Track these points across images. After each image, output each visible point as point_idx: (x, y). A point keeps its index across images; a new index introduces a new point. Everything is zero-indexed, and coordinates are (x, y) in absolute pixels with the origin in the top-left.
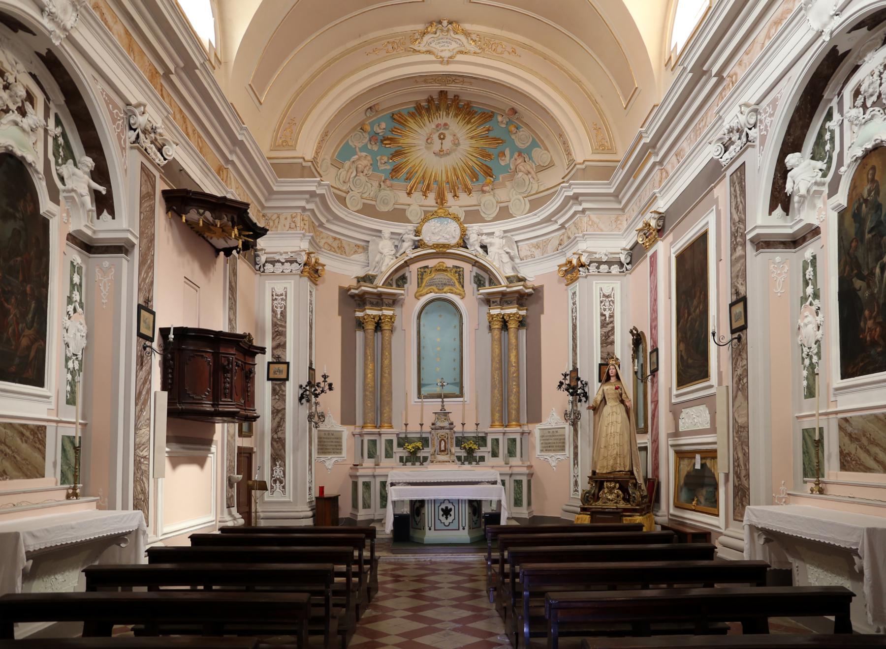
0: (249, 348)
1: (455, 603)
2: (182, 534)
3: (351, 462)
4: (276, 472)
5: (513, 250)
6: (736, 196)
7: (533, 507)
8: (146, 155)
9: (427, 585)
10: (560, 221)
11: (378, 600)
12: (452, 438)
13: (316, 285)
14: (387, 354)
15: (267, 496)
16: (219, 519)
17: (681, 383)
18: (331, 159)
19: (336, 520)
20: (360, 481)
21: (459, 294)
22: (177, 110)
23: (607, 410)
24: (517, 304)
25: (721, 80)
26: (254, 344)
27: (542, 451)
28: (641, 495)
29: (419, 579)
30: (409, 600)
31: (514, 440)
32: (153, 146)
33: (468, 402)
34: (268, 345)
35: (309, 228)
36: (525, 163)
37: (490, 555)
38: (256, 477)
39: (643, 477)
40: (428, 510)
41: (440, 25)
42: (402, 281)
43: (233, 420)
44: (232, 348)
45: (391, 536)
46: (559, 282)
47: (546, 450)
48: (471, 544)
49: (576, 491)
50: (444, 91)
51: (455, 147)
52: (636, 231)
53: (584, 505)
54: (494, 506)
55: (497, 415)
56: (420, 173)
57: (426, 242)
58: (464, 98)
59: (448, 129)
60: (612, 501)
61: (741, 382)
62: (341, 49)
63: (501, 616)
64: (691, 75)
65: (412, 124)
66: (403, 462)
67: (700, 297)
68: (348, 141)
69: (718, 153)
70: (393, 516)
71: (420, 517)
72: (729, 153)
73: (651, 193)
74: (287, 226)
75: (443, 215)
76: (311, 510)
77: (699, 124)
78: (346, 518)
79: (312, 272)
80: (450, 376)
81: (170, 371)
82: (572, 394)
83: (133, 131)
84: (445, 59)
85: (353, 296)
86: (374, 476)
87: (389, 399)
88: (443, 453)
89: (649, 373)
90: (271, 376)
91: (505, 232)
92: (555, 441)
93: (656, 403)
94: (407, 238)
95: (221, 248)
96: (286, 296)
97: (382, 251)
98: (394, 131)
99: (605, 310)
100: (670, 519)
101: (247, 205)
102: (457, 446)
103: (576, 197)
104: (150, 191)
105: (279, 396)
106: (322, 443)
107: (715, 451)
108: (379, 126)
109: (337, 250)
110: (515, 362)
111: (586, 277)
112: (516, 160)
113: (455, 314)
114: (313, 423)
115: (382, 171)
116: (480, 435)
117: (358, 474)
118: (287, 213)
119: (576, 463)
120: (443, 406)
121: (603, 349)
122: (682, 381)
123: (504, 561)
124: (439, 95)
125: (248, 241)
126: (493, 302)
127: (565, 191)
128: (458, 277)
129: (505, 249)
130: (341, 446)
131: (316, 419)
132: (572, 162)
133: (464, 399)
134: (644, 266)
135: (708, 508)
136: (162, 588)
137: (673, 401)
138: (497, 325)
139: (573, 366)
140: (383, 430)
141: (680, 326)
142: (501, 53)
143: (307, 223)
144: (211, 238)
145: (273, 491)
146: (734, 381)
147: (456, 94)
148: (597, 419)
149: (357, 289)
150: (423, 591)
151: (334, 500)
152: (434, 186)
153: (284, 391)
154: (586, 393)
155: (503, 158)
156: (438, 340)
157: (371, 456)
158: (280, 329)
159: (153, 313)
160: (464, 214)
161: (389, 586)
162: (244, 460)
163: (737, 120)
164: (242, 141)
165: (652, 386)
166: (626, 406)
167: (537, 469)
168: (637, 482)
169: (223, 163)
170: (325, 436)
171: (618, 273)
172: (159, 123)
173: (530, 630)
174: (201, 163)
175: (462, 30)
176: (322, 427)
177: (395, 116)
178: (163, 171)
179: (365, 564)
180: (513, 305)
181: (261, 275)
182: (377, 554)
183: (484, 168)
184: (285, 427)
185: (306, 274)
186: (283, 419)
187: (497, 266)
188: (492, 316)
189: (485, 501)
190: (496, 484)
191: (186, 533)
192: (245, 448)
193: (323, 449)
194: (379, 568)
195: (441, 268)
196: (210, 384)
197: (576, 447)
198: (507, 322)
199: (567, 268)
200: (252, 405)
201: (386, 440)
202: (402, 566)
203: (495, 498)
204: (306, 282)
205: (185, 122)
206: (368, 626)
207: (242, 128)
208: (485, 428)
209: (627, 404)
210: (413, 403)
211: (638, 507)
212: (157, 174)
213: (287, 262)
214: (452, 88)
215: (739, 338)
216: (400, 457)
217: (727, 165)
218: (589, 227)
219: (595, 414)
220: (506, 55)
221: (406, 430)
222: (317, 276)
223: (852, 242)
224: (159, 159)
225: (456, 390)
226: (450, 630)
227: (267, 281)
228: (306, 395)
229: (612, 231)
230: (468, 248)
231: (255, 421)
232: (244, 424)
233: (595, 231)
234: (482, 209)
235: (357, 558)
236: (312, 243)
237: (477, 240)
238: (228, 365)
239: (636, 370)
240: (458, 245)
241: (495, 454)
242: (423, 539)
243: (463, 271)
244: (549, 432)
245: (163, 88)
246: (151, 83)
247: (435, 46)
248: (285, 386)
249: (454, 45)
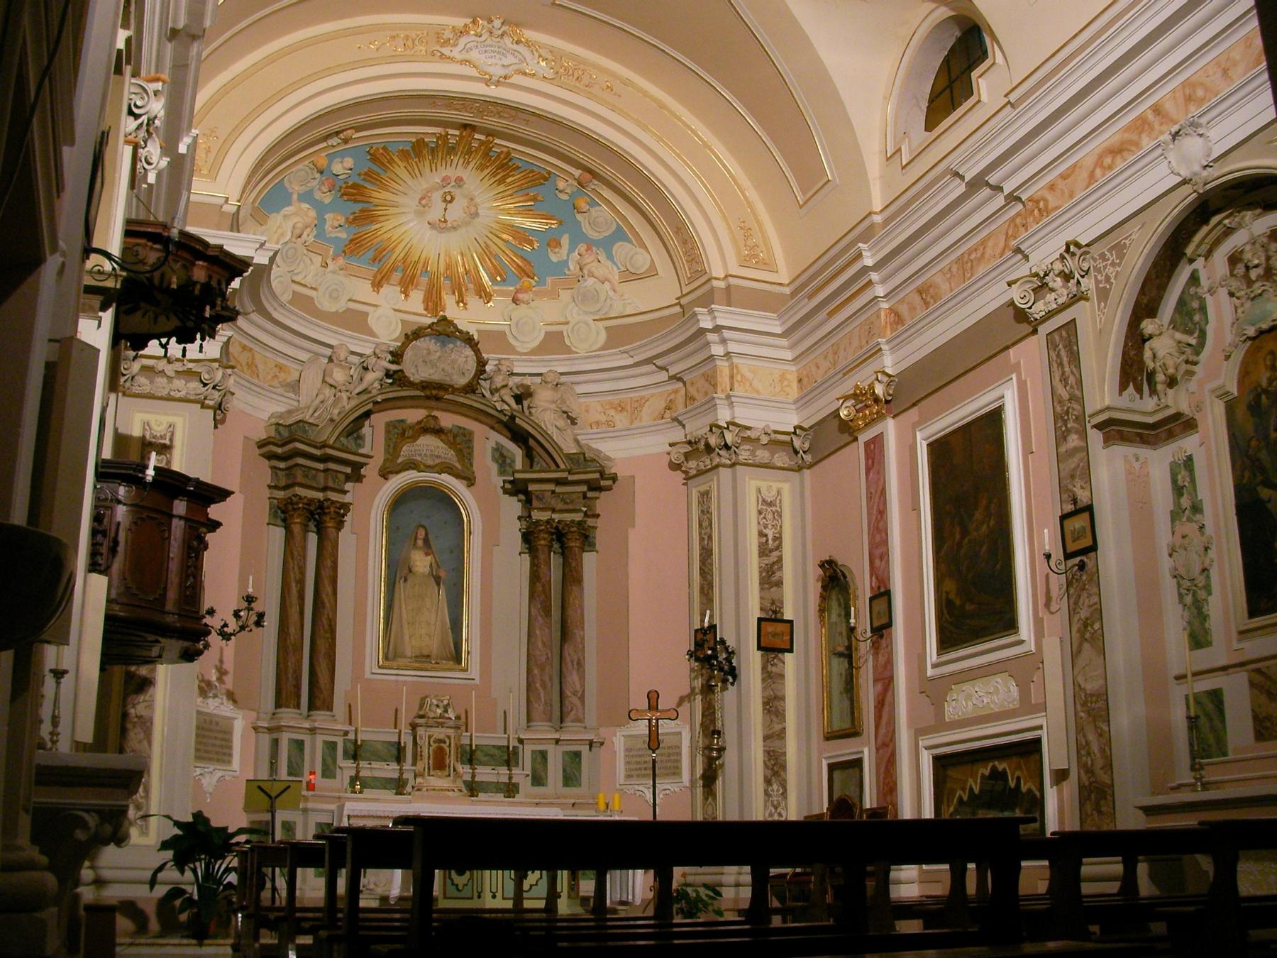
6: (1061, 365)
17: (946, 642)
27: (629, 776)
61: (1089, 628)
65: (400, 169)
83: (132, 118)
99: (766, 526)
107: (1038, 741)
130: (230, 748)
146: (1074, 629)
155: (557, 250)
201: (325, 742)
215: (1082, 566)
223: (1250, 440)
233: (746, 391)
241: (538, 780)
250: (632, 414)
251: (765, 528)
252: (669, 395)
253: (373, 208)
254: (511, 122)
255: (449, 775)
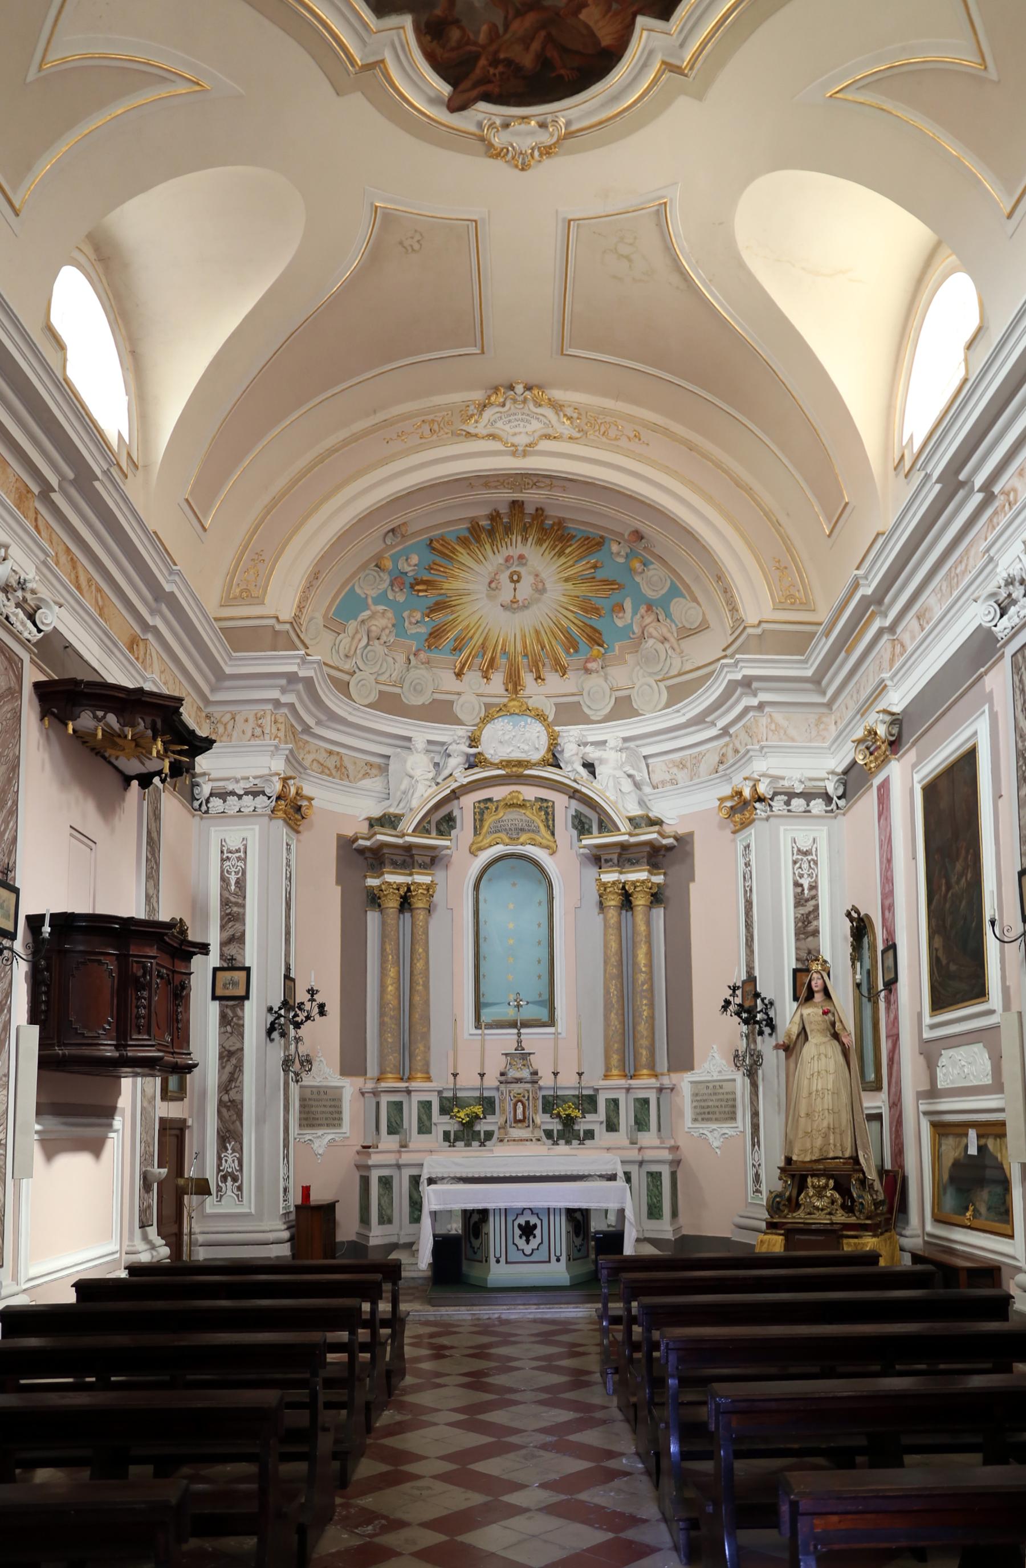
0: (181, 945)
1: (545, 1396)
2: (62, 1278)
3: (357, 1143)
4: (226, 1161)
5: (640, 771)
7: (682, 1219)
8: (7, 627)
9: (493, 1364)
10: (721, 723)
11: (405, 1391)
12: (535, 1099)
13: (298, 832)
14: (421, 950)
15: (210, 1205)
16: (125, 1248)
18: (325, 616)
19: (330, 1247)
20: (374, 1176)
21: (547, 847)
22: (61, 549)
23: (809, 1050)
24: (648, 864)
25: (989, 497)
26: (190, 938)
27: (695, 1120)
28: (873, 1200)
29: (480, 1353)
30: (461, 1391)
31: (646, 1102)
32: (19, 610)
33: (564, 1035)
34: (214, 938)
35: (286, 736)
36: (659, 624)
37: (605, 1307)
38: (191, 1172)
39: (876, 1166)
40: (494, 1228)
41: (512, 393)
42: (447, 824)
43: (152, 1072)
44: (151, 946)
45: (429, 1274)
46: (721, 827)
47: (703, 1119)
48: (572, 1287)
49: (758, 1191)
50: (518, 501)
51: (537, 595)
52: (853, 742)
53: (772, 1217)
54: (612, 1219)
55: (615, 1058)
56: (477, 640)
57: (488, 756)
58: (553, 513)
59: (525, 564)
60: (822, 1210)
62: (343, 434)
63: (628, 1421)
64: (938, 487)
65: (463, 556)
66: (449, 1141)
67: (966, 858)
68: (353, 586)
69: (990, 617)
70: (431, 1238)
71: (479, 1241)
72: (1009, 619)
73: (877, 680)
74: (249, 734)
75: (517, 711)
76: (288, 1228)
77: (956, 568)
78: (348, 1242)
79: (292, 811)
80: (532, 988)
81: (44, 989)
82: (746, 1022)
84: (520, 448)
85: (361, 851)
86: (399, 1166)
87: (425, 1030)
88: (520, 1125)
89: (881, 986)
90: (219, 992)
91: (625, 740)
92: (718, 1104)
93: (895, 1038)
94: (455, 751)
95: (132, 773)
96: (245, 852)
97: (412, 773)
98: (432, 569)
99: (801, 876)
100: (926, 1243)
101: (180, 700)
102: (544, 1111)
103: (747, 683)
104: (13, 684)
105: (233, 1027)
106: (307, 1109)
107: (1003, 1124)
108: (407, 560)
109: (334, 772)
110: (645, 965)
111: (767, 819)
112: (643, 617)
113: (540, 882)
114: (291, 1074)
115: (413, 637)
116: (585, 1092)
117: (370, 1163)
118: (249, 712)
119: (755, 1142)
120: (519, 1042)
121: (798, 943)
122: (940, 1001)
123: (633, 1320)
124: (510, 508)
125: (180, 761)
126: (606, 861)
127: (727, 672)
128: (544, 817)
129: (625, 769)
131: (297, 1066)
132: (739, 624)
133: (557, 1030)
134: (868, 802)
135: (993, 1224)
136: (22, 1382)
137: (926, 1035)
138: (613, 901)
139: (748, 972)
140: (414, 1085)
141: (932, 908)
142: (616, 439)
143: (282, 727)
144: (117, 758)
145: (221, 1196)
147: (539, 506)
148: (792, 1065)
149: (368, 839)
150: (487, 1375)
151: (328, 1210)
152: (502, 662)
153: (242, 1018)
154: (771, 1019)
155: (621, 615)
156: (511, 926)
157: (392, 1130)
158: (235, 909)
159: (16, 891)
160: (554, 709)
161: (426, 1366)
162: (171, 1142)
163: (1020, 566)
164: (172, 593)
165: (888, 1009)
166: (842, 1044)
167: (687, 1152)
168: (865, 1177)
169: (138, 631)
170: (313, 1097)
171: (823, 813)
172: (30, 573)
173: (680, 1447)
174: (99, 632)
175: (549, 399)
176: (307, 1080)
177: (435, 544)
178: (36, 651)
179: (382, 1327)
180: (641, 865)
181: (202, 818)
182: (403, 1307)
183: (588, 630)
184: (242, 1082)
185: (280, 814)
186: (239, 1067)
187: (612, 798)
188: (604, 885)
189: (596, 1210)
190: (615, 1179)
191: (68, 1276)
192: (172, 1121)
193: (310, 1119)
194: (407, 1333)
195: (515, 801)
196: (112, 1011)
197: (755, 1114)
198: (630, 895)
199: (734, 803)
200: (185, 1045)
201: (420, 1102)
202: (447, 1328)
203: (613, 1206)
204: (280, 829)
205: (74, 568)
206: (388, 1442)
207: (171, 572)
208: (594, 1080)
209: (845, 1040)
210: (466, 1036)
211: (868, 1222)
212: (25, 656)
213: (247, 793)
214: (532, 497)
216: (444, 1132)
217: (1005, 639)
218: (771, 733)
219: (787, 1057)
220: (623, 442)
221: (455, 1084)
222: (299, 817)
224: (29, 632)
225: (543, 1014)
226: (535, 1447)
227: (213, 829)
228: (280, 1024)
229: (810, 741)
230: (561, 768)
231: (189, 1073)
232: (170, 1078)
233: (781, 740)
234: (585, 701)
235: (368, 1317)
236: (289, 761)
237: (577, 754)
238: (144, 975)
239: (858, 981)
240: (544, 763)
241: (612, 1126)
242: (486, 1280)
243: (553, 807)
244: (707, 1087)
245: (39, 517)
246: (19, 509)
247: (502, 427)
248: (243, 1010)
249: (535, 425)
250: (692, 770)
251: (800, 878)
252: (721, 749)
253: (448, 599)
254: (549, 491)
255: (529, 1126)
